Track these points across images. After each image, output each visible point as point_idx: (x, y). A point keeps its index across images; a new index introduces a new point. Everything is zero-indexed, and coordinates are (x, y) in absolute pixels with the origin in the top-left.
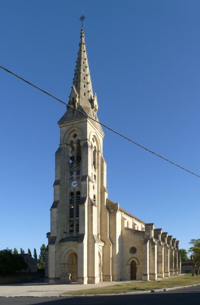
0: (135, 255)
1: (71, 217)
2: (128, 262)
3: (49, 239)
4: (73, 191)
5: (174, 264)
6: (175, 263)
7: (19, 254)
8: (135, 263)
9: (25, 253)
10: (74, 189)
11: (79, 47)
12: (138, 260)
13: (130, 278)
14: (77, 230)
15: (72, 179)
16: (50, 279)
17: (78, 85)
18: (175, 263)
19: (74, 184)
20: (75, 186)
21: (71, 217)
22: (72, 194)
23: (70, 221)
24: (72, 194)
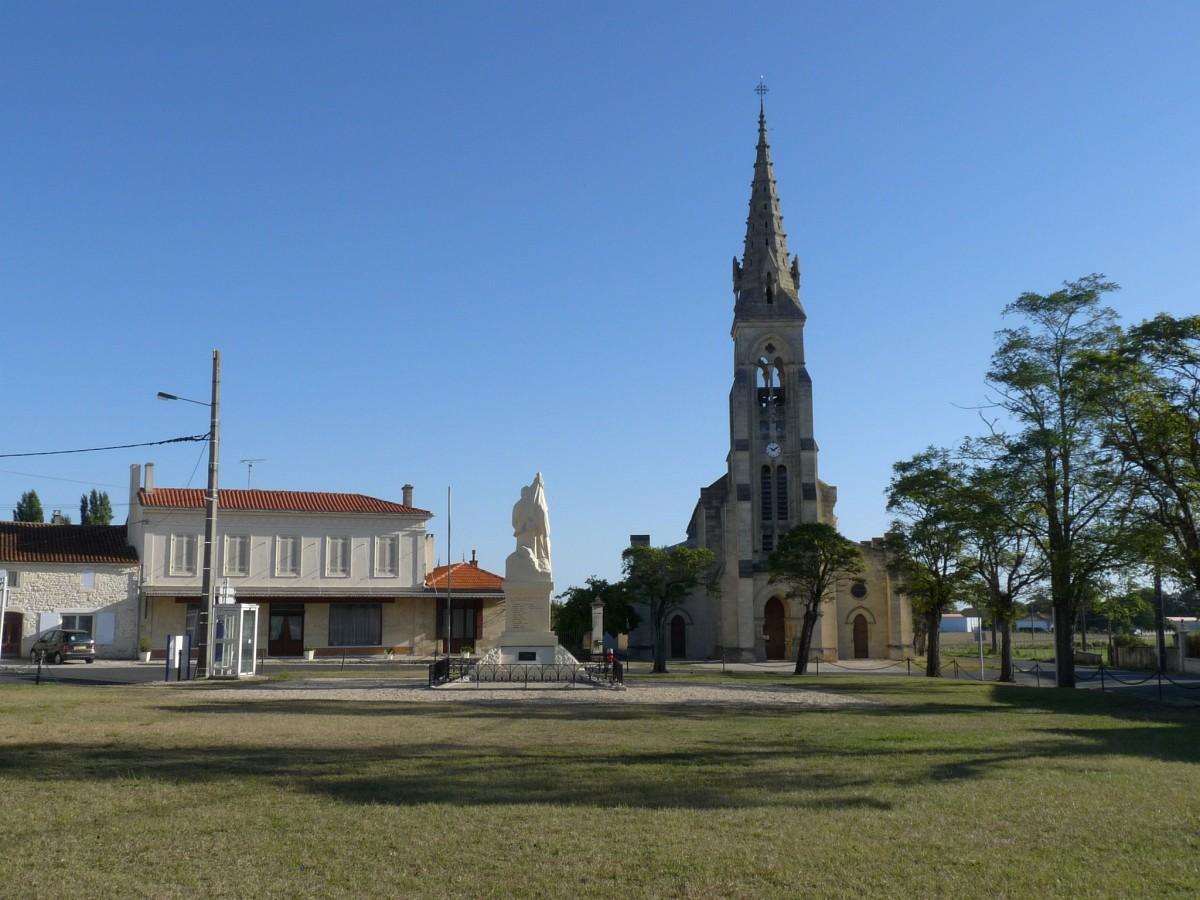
0: (865, 603)
1: (764, 519)
2: (848, 617)
3: (521, 500)
4: (769, 463)
5: (1158, 725)
6: (193, 496)
7: (146, 535)
8: (865, 619)
9: (73, 523)
10: (773, 461)
11: (768, 141)
12: (871, 613)
13: (853, 655)
14: (770, 541)
15: (766, 438)
16: (743, 650)
17: (770, 241)
18: (193, 496)
19: (773, 450)
20: (775, 454)
21: (764, 519)
22: (766, 469)
23: (763, 527)
24: (766, 469)
